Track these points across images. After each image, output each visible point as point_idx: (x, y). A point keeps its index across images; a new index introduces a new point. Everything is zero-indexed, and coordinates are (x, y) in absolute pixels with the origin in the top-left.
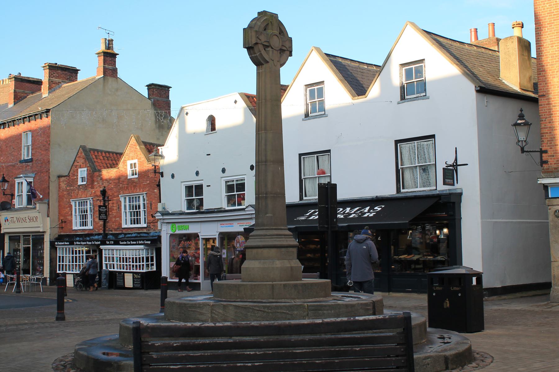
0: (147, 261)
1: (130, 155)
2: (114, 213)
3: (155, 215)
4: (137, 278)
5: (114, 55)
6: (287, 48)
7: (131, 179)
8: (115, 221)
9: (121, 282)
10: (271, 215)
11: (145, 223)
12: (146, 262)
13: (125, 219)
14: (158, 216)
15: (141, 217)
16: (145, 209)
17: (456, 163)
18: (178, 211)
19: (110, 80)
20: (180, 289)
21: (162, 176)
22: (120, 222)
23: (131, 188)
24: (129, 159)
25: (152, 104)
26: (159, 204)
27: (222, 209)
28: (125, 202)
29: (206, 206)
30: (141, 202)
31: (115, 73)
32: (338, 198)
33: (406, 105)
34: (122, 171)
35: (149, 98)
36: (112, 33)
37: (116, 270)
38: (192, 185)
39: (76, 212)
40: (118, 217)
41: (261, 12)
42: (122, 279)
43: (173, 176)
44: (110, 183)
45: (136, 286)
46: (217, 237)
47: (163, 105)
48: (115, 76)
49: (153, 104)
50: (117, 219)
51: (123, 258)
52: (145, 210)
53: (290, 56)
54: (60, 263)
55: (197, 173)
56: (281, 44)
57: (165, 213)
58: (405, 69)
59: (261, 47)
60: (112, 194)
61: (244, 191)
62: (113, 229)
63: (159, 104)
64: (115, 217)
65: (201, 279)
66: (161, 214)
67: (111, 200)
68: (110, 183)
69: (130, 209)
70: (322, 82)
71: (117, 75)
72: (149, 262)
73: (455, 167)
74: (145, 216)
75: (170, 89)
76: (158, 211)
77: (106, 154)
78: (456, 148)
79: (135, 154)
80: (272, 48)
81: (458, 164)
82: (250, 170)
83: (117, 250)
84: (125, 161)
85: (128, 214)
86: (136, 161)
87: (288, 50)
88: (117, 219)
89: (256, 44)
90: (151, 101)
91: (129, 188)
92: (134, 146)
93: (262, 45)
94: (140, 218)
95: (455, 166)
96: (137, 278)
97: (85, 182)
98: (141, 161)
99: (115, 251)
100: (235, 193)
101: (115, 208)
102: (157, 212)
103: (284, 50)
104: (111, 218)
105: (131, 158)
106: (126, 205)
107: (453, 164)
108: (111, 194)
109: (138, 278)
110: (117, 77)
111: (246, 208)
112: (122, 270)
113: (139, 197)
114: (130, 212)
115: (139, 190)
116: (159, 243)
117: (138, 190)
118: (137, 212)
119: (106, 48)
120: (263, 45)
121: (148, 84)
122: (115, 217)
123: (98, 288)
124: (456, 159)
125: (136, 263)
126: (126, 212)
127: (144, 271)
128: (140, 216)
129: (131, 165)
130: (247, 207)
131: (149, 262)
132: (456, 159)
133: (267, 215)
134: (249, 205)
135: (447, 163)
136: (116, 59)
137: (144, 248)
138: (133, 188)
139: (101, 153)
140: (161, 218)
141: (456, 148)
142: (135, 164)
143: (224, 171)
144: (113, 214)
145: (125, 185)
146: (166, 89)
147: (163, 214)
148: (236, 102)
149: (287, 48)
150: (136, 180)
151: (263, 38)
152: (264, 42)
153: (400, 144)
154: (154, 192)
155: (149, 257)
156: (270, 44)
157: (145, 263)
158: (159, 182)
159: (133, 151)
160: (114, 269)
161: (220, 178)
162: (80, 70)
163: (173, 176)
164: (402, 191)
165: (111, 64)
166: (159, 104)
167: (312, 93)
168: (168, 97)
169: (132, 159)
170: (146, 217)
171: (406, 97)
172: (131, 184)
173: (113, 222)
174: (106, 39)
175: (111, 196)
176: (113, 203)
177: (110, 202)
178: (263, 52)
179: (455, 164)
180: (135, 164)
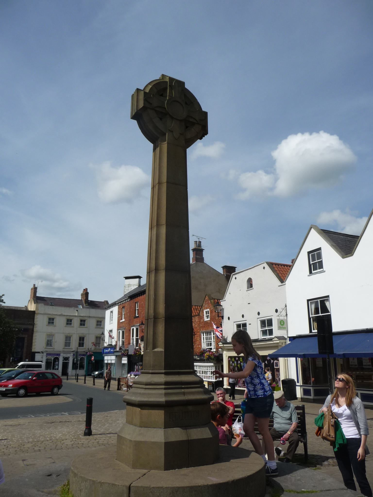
2: (198, 342)
5: (202, 250)
8: (199, 348)
19: (200, 264)
20: (279, 404)
23: (207, 326)
24: (205, 309)
27: (259, 340)
28: (203, 335)
33: (313, 276)
39: (204, 340)
43: (229, 318)
44: (195, 324)
55: (243, 316)
58: (311, 255)
64: (198, 345)
66: (222, 343)
68: (195, 324)
70: (320, 249)
71: (204, 262)
77: (195, 307)
82: (258, 315)
83: (199, 366)
86: (209, 310)
88: (200, 346)
91: (206, 327)
92: (208, 300)
97: (209, 318)
99: (198, 367)
101: (198, 339)
106: (272, 329)
117: (210, 328)
119: (197, 247)
121: (222, 266)
123: (333, 420)
126: (133, 339)
129: (206, 312)
133: (156, 350)
134: (275, 337)
138: (207, 327)
139: (217, 300)
140: (222, 345)
142: (208, 311)
143: (259, 314)
147: (223, 344)
148: (264, 268)
150: (209, 322)
153: (310, 301)
159: (207, 304)
161: (233, 323)
162: (204, 250)
163: (229, 318)
164: (313, 331)
167: (313, 256)
169: (207, 309)
171: (313, 272)
172: (207, 324)
174: (197, 242)
175: (196, 332)
176: (197, 337)
177: (195, 336)
180: (208, 311)
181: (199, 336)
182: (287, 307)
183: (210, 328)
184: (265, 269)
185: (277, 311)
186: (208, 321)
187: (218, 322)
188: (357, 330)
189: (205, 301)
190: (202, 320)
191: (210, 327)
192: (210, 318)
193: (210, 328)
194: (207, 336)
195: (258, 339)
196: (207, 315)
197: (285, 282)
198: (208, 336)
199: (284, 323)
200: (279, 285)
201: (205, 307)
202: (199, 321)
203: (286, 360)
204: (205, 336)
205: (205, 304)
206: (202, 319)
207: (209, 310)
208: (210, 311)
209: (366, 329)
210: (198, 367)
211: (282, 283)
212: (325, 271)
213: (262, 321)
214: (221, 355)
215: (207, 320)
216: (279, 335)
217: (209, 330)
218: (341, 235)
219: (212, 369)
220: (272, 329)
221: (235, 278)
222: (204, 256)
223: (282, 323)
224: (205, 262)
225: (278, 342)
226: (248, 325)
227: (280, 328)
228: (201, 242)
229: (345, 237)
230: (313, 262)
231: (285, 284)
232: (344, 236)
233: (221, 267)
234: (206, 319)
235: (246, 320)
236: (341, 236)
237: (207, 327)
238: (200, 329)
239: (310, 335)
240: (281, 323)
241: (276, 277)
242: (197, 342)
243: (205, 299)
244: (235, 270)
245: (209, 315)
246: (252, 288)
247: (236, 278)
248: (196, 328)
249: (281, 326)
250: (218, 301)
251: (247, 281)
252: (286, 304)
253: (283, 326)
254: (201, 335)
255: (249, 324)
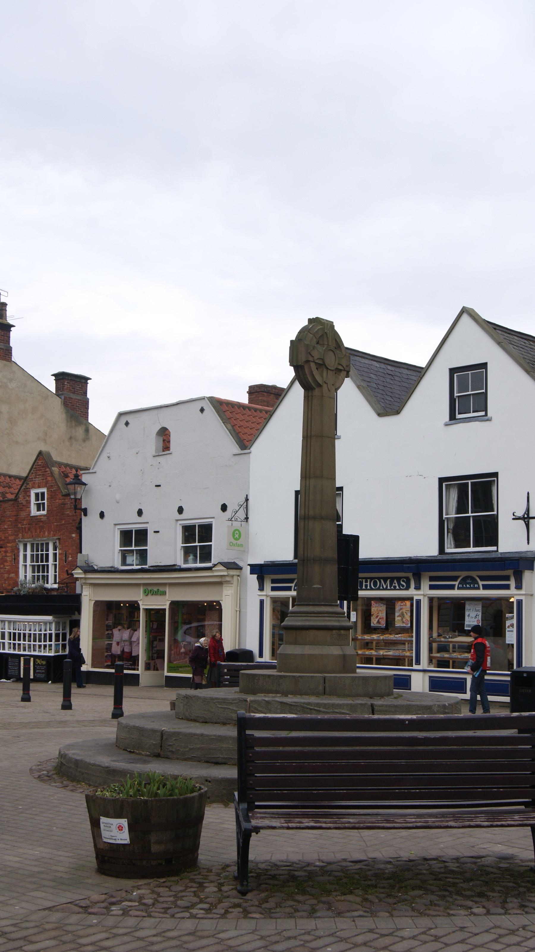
0: (57, 640)
1: (35, 480)
2: (7, 566)
3: (73, 572)
4: (40, 665)
6: (343, 367)
7: (37, 516)
9: (15, 670)
10: (320, 586)
11: (55, 583)
12: (56, 641)
13: (24, 576)
14: (78, 573)
15: (50, 574)
16: (56, 561)
17: (528, 514)
18: (108, 567)
21: (86, 515)
22: (16, 580)
24: (33, 487)
25: (61, 404)
26: (79, 554)
27: (177, 567)
28: (25, 550)
29: (152, 561)
30: (51, 552)
31: (9, 355)
32: (360, 557)
34: (22, 503)
35: (58, 394)
36: (6, 294)
37: (7, 651)
38: (131, 529)
40: (13, 573)
41: (313, 318)
42: (16, 666)
43: (102, 515)
45: (38, 676)
46: (167, 607)
47: (78, 405)
48: (9, 360)
49: (63, 403)
50: (12, 575)
51: (19, 634)
52: (56, 564)
53: (346, 377)
54: (30, 642)
55: (140, 513)
56: (337, 363)
57: (89, 569)
59: (313, 365)
60: (5, 538)
61: (211, 541)
62: (5, 590)
63: (72, 403)
64: (9, 572)
65: (140, 671)
66: (82, 570)
67: (3, 546)
69: (32, 561)
71: (11, 358)
72: (59, 641)
73: (526, 520)
74: (56, 572)
75: (89, 381)
76: (78, 566)
78: (528, 494)
79: (43, 480)
80: (327, 368)
81: (531, 515)
83: (10, 622)
84: (27, 489)
85: (29, 569)
86: (45, 490)
87: (345, 370)
88: (12, 575)
89: (308, 362)
90: (60, 398)
93: (314, 363)
94: (48, 576)
95: (526, 518)
96: (40, 665)
97: (44, 510)
98: (52, 490)
99: (7, 624)
100: (197, 544)
101: (8, 559)
102: (77, 567)
103: (341, 370)
104: (2, 573)
105: (37, 485)
107: (524, 516)
108: (3, 538)
109: (42, 665)
110: (11, 360)
111: (213, 567)
112: (16, 652)
113: (47, 544)
114: (32, 565)
115: (49, 533)
116: (76, 613)
117: (46, 533)
118: (43, 566)
120: (316, 363)
121: (56, 372)
122: (9, 572)
124: (528, 510)
125: (39, 642)
126: (26, 566)
127: (52, 654)
128: (48, 572)
129: (37, 495)
130: (215, 565)
131: (59, 641)
132: (528, 510)
135: (515, 514)
136: (10, 333)
137: (54, 620)
138: (38, 531)
140: (83, 576)
141: (528, 494)
142: (43, 494)
143: (180, 510)
144: (6, 568)
145: (26, 525)
146: (83, 381)
147: (86, 572)
148: (202, 410)
149: (343, 367)
150: (43, 519)
151: (316, 355)
152: (318, 359)
154: (72, 538)
155: (59, 634)
156: (324, 362)
157: (53, 643)
158: (80, 522)
160: (5, 650)
161: (175, 521)
163: (102, 515)
165: (3, 340)
166: (72, 403)
168: (85, 393)
169: (39, 487)
170: (57, 574)
171: (458, 416)
172: (36, 524)
173: (5, 580)
178: (316, 373)
179: (526, 516)
180: (43, 494)
181: (12, 551)
182: (248, 501)
183: (46, 533)
184: (205, 412)
185: (224, 508)
186: (42, 517)
187: (71, 521)
188: (389, 559)
189: (34, 467)
190: (23, 514)
191: (44, 531)
192: (47, 511)
193: (44, 533)
194: (44, 553)
195: (174, 565)
196: (40, 502)
197: (249, 449)
198: (40, 553)
199: (240, 536)
200: (235, 454)
201: (34, 483)
202: (15, 516)
203: (238, 612)
204: (29, 553)
205: (36, 475)
206: (23, 510)
207: (45, 490)
208: (47, 494)
209: (407, 558)
210: (7, 624)
211: (242, 450)
212: (340, 436)
213: (186, 526)
214: (77, 599)
215: (38, 513)
216: (226, 561)
217: (43, 537)
218: (375, 361)
219: (48, 629)
220: (211, 545)
221: (125, 422)
222: (11, 344)
223: (237, 536)
224: (13, 360)
225: (225, 573)
226: (150, 536)
227: (231, 544)
228: (7, 305)
229: (383, 366)
230: (457, 514)
231: (250, 453)
232: (380, 362)
233: (52, 375)
234: (34, 511)
235: (148, 523)
236: (375, 362)
237: (38, 531)
238: (18, 535)
239: (293, 563)
240: (234, 535)
241: (229, 434)
242: (4, 566)
243: (36, 464)
244: (87, 385)
245: (45, 501)
246: (168, 452)
247: (127, 424)
248: (3, 531)
249: (235, 542)
250: (77, 471)
251: (88, 402)
252: (247, 495)
253: (239, 542)
254: (18, 549)
255: (155, 532)
